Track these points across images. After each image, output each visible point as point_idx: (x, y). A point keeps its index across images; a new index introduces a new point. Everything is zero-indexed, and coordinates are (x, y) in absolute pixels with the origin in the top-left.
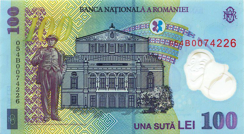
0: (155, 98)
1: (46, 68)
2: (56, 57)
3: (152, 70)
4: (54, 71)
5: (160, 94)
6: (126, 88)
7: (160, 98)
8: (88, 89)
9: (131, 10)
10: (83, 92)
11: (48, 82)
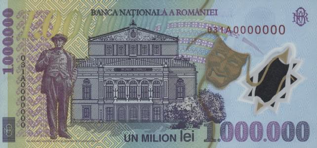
0: (186, 110)
1: (52, 75)
2: (65, 61)
3: (182, 77)
4: (62, 78)
5: (192, 105)
6: (150, 98)
7: (192, 111)
8: (104, 99)
9: (151, 13)
10: (98, 103)
11: (54, 92)
